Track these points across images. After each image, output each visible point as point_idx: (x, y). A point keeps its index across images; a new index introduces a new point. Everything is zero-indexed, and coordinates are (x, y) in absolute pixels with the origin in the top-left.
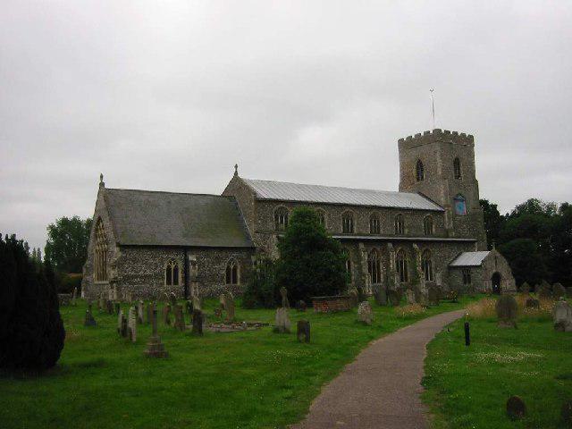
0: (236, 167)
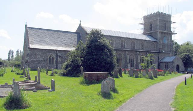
0: (80, 21)
